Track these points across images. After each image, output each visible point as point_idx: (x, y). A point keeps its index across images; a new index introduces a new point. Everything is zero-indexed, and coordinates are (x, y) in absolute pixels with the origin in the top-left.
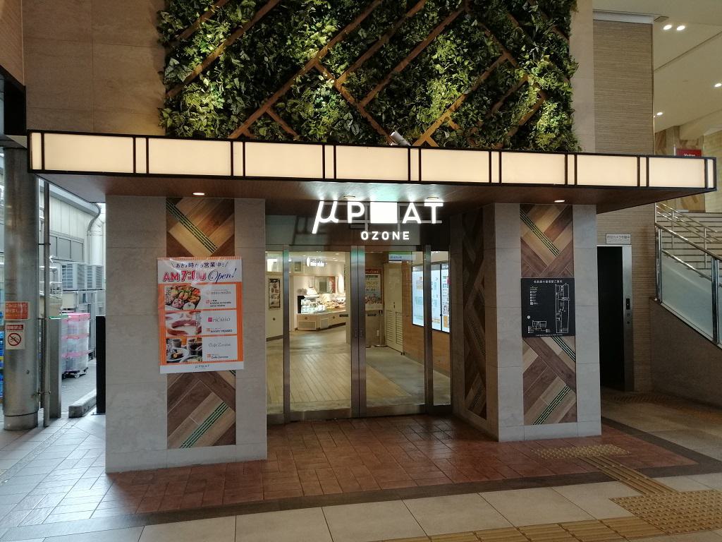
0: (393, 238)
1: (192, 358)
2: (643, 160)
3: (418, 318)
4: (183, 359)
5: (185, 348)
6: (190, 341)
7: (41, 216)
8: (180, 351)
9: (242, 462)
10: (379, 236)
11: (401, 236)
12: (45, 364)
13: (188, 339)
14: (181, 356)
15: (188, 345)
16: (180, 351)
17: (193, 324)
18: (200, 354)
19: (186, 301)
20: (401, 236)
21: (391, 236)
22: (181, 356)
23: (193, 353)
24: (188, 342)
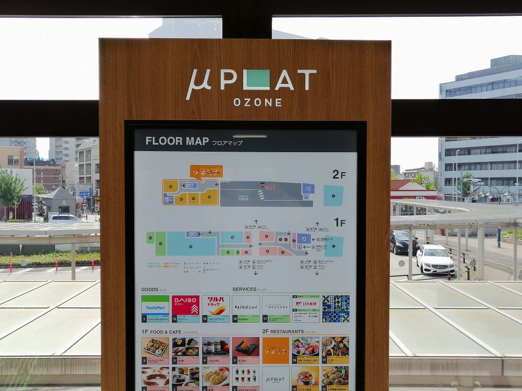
0: (266, 105)
1: (191, 382)
2: (97, 257)
3: (414, 262)
4: (185, 383)
5: (187, 375)
6: (190, 370)
7: (190, 141)
8: (183, 376)
9: (514, 80)
10: (251, 103)
11: (274, 103)
12: (411, 200)
13: (189, 368)
14: (183, 380)
15: (188, 373)
16: (183, 376)
17: (162, 376)
18: (198, 379)
19: (158, 348)
20: (274, 103)
21: (263, 102)
22: (183, 380)
23: (192, 378)
24: (189, 371)
